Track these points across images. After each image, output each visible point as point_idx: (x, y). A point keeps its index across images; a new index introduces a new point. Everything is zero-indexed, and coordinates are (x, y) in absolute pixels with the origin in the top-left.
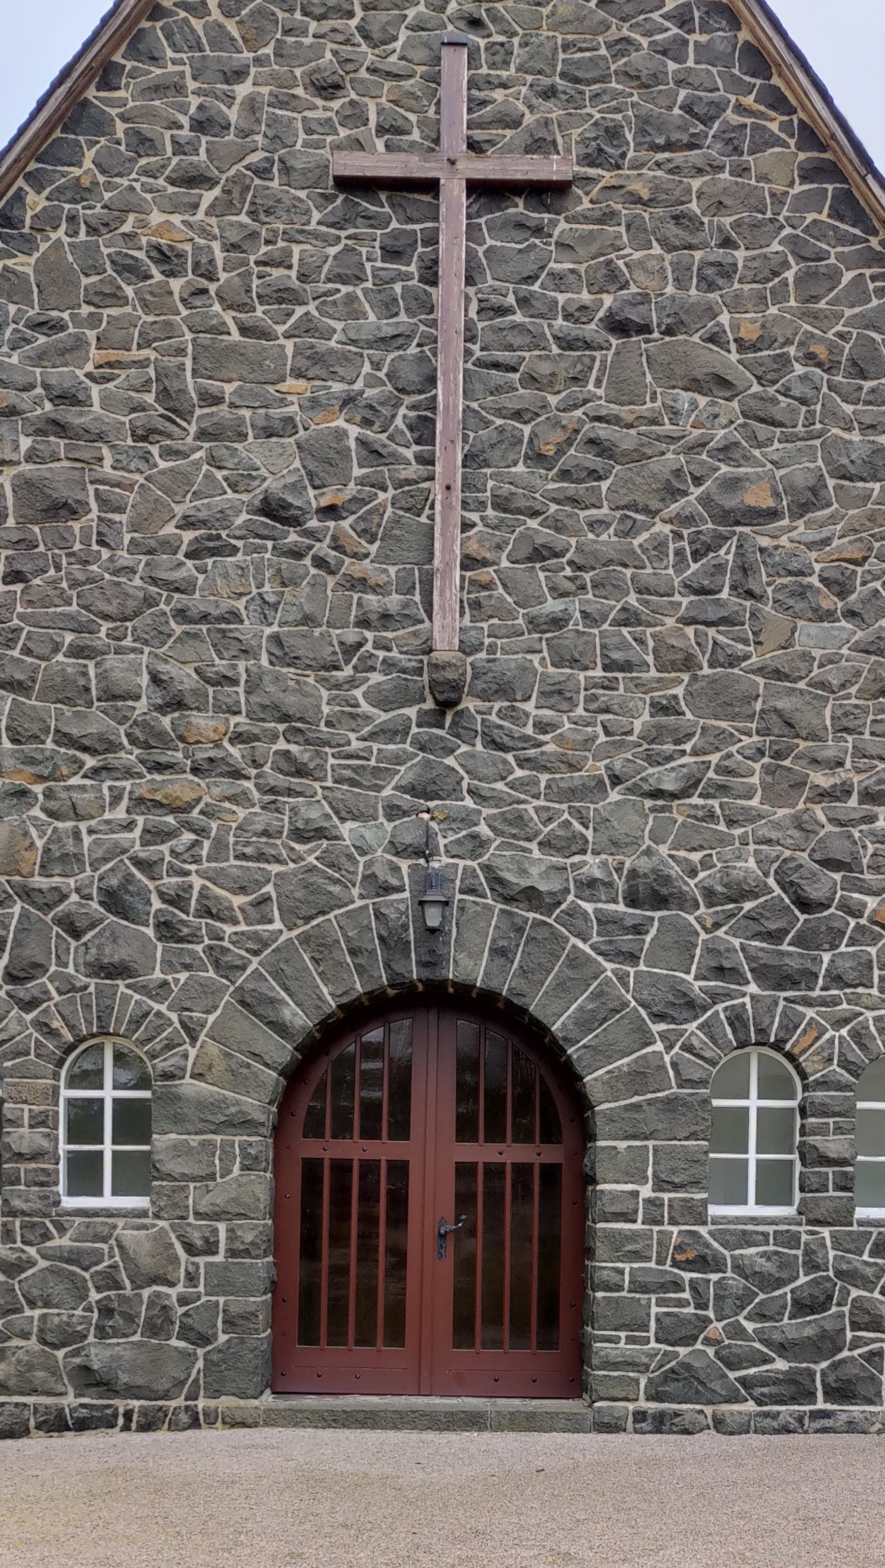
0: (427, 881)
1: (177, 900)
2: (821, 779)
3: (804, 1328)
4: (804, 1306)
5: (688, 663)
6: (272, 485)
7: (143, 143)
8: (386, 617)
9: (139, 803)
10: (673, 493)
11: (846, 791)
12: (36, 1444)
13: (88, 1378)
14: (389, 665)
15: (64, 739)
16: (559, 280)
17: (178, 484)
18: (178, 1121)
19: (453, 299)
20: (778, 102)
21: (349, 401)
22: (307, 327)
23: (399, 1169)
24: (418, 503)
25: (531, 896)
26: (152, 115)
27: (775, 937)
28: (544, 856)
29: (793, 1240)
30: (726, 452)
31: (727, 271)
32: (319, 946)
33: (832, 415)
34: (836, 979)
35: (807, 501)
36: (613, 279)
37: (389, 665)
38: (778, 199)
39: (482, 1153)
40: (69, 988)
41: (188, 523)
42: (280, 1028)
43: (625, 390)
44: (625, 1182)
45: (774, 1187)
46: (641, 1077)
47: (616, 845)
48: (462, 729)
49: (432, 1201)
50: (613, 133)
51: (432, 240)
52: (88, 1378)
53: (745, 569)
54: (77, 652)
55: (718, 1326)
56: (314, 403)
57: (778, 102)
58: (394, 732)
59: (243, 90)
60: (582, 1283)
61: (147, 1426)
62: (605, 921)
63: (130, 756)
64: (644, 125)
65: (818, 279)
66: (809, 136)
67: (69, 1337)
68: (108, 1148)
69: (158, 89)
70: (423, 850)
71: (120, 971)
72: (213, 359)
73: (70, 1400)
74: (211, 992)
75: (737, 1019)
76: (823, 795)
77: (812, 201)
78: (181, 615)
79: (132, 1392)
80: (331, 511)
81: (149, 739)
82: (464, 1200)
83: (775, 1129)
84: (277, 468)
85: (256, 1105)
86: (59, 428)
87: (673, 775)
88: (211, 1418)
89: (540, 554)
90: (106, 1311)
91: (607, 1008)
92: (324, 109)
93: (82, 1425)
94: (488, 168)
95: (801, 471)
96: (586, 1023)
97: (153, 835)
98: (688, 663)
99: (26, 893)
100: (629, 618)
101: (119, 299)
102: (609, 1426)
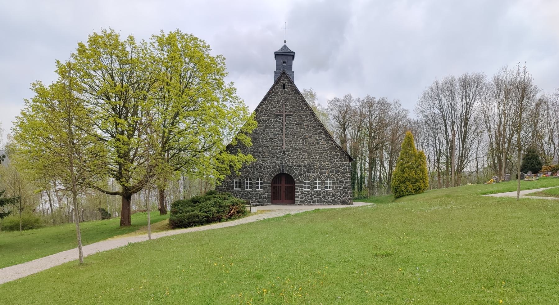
0: (283, 166)
7: (261, 112)
17: (264, 137)
19: (284, 123)
20: (308, 108)
24: (282, 138)
28: (290, 163)
35: (311, 137)
36: (296, 121)
43: (297, 129)
44: (298, 188)
45: (309, 187)
48: (285, 154)
49: (283, 189)
60: (295, 195)
65: (311, 121)
67: (257, 199)
70: (282, 163)
72: (267, 128)
81: (262, 155)
82: (286, 189)
83: (309, 183)
84: (271, 136)
87: (437, 111)
91: (296, 174)
92: (275, 109)
94: (287, 114)
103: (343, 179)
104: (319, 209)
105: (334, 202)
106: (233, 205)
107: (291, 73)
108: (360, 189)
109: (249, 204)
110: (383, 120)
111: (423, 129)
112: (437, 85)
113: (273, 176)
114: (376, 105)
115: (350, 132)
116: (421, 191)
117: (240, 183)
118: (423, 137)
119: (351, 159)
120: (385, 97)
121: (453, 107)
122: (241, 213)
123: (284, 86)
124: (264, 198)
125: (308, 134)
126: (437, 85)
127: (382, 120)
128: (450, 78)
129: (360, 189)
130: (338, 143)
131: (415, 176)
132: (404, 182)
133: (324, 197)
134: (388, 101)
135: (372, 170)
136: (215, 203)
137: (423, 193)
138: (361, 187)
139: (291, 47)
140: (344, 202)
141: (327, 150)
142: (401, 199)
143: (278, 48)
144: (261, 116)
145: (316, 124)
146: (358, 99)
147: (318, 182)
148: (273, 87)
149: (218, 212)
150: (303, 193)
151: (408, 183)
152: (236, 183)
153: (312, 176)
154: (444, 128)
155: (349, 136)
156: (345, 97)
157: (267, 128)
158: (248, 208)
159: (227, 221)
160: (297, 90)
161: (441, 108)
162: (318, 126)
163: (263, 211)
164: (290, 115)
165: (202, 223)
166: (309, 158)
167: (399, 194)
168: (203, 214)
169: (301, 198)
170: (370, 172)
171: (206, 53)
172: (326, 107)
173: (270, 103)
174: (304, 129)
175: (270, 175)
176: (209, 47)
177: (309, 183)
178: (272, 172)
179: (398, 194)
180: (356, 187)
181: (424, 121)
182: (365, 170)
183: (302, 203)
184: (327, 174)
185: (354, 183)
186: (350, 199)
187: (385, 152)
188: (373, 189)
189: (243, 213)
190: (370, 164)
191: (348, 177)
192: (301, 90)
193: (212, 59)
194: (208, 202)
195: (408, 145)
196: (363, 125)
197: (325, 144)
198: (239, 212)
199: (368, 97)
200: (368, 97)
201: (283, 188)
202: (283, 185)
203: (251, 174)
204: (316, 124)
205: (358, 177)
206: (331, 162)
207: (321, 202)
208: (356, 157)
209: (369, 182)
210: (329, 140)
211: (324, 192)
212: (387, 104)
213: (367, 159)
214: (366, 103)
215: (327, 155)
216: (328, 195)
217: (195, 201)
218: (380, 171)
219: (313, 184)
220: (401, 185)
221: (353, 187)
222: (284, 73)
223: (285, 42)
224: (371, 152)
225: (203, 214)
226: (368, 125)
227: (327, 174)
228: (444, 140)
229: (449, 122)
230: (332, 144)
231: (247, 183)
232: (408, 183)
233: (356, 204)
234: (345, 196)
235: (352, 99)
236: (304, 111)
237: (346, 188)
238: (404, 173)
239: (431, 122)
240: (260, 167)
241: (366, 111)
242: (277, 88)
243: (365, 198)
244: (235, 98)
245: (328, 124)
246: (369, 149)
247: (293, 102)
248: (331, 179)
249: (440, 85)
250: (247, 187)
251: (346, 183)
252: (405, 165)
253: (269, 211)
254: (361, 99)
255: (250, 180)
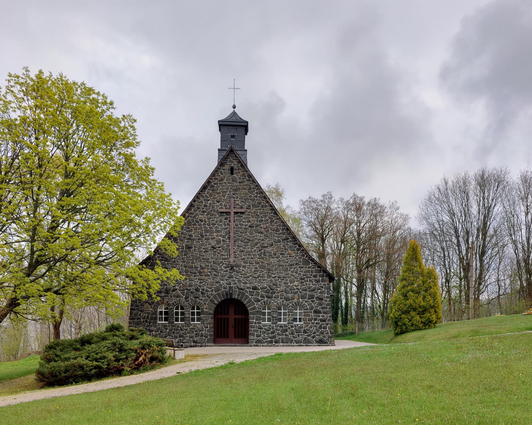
0: (230, 288)
1: (203, 290)
2: (273, 276)
3: (272, 335)
4: (272, 333)
5: (259, 263)
6: (213, 245)
7: (198, 208)
8: (225, 259)
9: (199, 279)
10: (256, 245)
11: (276, 277)
12: (189, 348)
13: (194, 342)
14: (226, 264)
15: (190, 272)
16: (244, 222)
17: (202, 245)
18: (204, 314)
19: (232, 224)
20: (268, 202)
21: (221, 235)
22: (216, 227)
23: (228, 319)
25: (241, 289)
26: (199, 205)
27: (268, 293)
29: (270, 326)
30: (262, 240)
31: (262, 221)
32: (219, 294)
33: (274, 236)
34: (275, 298)
36: (250, 222)
37: (226, 264)
38: (268, 213)
39: (237, 317)
40: (191, 299)
41: (204, 249)
42: (215, 304)
43: (251, 233)
44: (253, 321)
45: (269, 320)
46: (254, 308)
47: (251, 283)
48: (234, 271)
49: (232, 322)
50: (249, 206)
51: (230, 218)
52: (194, 342)
53: (264, 253)
54: (192, 263)
55: (262, 335)
56: (217, 236)
57: (268, 202)
58: (227, 271)
59: (209, 202)
60: (248, 331)
61: (201, 347)
62: (250, 292)
63: (198, 274)
64: (253, 205)
65: (272, 222)
66: (271, 206)
67: (192, 337)
68: (196, 317)
69: (200, 202)
70: (230, 284)
71: (197, 297)
73: (192, 344)
74: (207, 300)
75: (264, 302)
76: (273, 277)
77: (270, 213)
78: (203, 259)
79: (199, 343)
80: (219, 247)
81: (200, 272)
83: (269, 314)
84: (213, 243)
85: (212, 312)
86: (189, 239)
87: (446, 218)
88: (208, 346)
89: (242, 251)
90: (196, 334)
91: (250, 301)
92: (218, 204)
93: (194, 347)
94: (236, 210)
95: (270, 242)
96: (248, 302)
97: (200, 283)
98: (259, 263)
99: (187, 289)
100: (252, 258)
101: (196, 225)
102: (251, 346)
103: (319, 308)
104: (280, 354)
105: (307, 342)
106: (143, 348)
107: (243, 152)
108: (345, 322)
109: (172, 346)
110: (376, 227)
111: (427, 241)
112: (446, 183)
113: (216, 302)
114: (365, 208)
115: (331, 244)
116: (432, 325)
117: (166, 313)
118: (427, 252)
119: (331, 278)
120: (377, 198)
121: (467, 213)
122: (157, 361)
123: (232, 170)
124: (202, 335)
125: (267, 242)
126: (446, 183)
127: (373, 229)
128: (463, 174)
129: (345, 322)
130: (315, 256)
131: (422, 303)
132: (407, 312)
133: (292, 334)
134: (381, 202)
135: (361, 295)
136: (114, 344)
137: (435, 327)
138: (346, 319)
139: (243, 115)
140: (321, 342)
141: (297, 264)
142: (404, 336)
143: (224, 116)
144: (197, 215)
145: (279, 226)
146: (342, 200)
147: (282, 311)
148: (216, 171)
149: (118, 360)
150: (261, 328)
151: (412, 316)
152: (161, 313)
153: (274, 303)
154: (454, 240)
155: (329, 250)
156: (324, 196)
157: (206, 231)
158: (169, 351)
159: (132, 374)
160: (258, 186)
161: (452, 214)
162: (283, 229)
163: (195, 357)
164: (242, 213)
165: (88, 378)
166: (269, 276)
167: (401, 329)
168: (90, 363)
169: (258, 336)
170: (359, 298)
171: (108, 113)
172: (298, 210)
173: (211, 195)
174: (261, 233)
175: (212, 301)
176: (111, 103)
177: (269, 314)
178: (215, 297)
179: (398, 330)
180: (340, 319)
181: (427, 232)
182: (352, 295)
183: (259, 343)
184: (295, 300)
185: (337, 314)
186: (330, 337)
187: (377, 273)
188: (362, 322)
189: (160, 361)
190: (358, 287)
191: (328, 305)
192: (264, 186)
193: (117, 122)
194: (104, 343)
195: (412, 259)
196: (348, 234)
197: (294, 255)
198: (152, 359)
199: (355, 197)
200: (355, 197)
201: (231, 322)
202: (232, 317)
203: (183, 299)
204: (279, 226)
205: (342, 306)
206: (302, 283)
207: (287, 342)
208: (340, 276)
209: (357, 312)
210: (298, 250)
211: (292, 327)
212: (381, 206)
213: (354, 280)
214: (352, 205)
215: (296, 273)
216: (298, 331)
217: (85, 341)
218: (372, 298)
219: (275, 316)
220: (403, 316)
221: (335, 319)
222: (232, 151)
223: (234, 107)
224: (360, 271)
225: (90, 363)
226: (355, 234)
227: (295, 300)
228: (455, 255)
229: (462, 233)
230: (303, 256)
231: (177, 314)
232: (413, 313)
233: (341, 345)
234: (322, 333)
235: (333, 199)
236: (262, 206)
237: (324, 321)
238: (407, 299)
239: (437, 234)
240: (197, 290)
241: (352, 215)
242: (222, 173)
243: (352, 334)
244: (152, 183)
245: (300, 233)
246: (357, 266)
247: (246, 194)
248: (302, 307)
249: (450, 183)
250: (177, 320)
251: (324, 313)
252: (409, 288)
253: (204, 356)
254: (345, 200)
255: (182, 308)
